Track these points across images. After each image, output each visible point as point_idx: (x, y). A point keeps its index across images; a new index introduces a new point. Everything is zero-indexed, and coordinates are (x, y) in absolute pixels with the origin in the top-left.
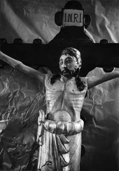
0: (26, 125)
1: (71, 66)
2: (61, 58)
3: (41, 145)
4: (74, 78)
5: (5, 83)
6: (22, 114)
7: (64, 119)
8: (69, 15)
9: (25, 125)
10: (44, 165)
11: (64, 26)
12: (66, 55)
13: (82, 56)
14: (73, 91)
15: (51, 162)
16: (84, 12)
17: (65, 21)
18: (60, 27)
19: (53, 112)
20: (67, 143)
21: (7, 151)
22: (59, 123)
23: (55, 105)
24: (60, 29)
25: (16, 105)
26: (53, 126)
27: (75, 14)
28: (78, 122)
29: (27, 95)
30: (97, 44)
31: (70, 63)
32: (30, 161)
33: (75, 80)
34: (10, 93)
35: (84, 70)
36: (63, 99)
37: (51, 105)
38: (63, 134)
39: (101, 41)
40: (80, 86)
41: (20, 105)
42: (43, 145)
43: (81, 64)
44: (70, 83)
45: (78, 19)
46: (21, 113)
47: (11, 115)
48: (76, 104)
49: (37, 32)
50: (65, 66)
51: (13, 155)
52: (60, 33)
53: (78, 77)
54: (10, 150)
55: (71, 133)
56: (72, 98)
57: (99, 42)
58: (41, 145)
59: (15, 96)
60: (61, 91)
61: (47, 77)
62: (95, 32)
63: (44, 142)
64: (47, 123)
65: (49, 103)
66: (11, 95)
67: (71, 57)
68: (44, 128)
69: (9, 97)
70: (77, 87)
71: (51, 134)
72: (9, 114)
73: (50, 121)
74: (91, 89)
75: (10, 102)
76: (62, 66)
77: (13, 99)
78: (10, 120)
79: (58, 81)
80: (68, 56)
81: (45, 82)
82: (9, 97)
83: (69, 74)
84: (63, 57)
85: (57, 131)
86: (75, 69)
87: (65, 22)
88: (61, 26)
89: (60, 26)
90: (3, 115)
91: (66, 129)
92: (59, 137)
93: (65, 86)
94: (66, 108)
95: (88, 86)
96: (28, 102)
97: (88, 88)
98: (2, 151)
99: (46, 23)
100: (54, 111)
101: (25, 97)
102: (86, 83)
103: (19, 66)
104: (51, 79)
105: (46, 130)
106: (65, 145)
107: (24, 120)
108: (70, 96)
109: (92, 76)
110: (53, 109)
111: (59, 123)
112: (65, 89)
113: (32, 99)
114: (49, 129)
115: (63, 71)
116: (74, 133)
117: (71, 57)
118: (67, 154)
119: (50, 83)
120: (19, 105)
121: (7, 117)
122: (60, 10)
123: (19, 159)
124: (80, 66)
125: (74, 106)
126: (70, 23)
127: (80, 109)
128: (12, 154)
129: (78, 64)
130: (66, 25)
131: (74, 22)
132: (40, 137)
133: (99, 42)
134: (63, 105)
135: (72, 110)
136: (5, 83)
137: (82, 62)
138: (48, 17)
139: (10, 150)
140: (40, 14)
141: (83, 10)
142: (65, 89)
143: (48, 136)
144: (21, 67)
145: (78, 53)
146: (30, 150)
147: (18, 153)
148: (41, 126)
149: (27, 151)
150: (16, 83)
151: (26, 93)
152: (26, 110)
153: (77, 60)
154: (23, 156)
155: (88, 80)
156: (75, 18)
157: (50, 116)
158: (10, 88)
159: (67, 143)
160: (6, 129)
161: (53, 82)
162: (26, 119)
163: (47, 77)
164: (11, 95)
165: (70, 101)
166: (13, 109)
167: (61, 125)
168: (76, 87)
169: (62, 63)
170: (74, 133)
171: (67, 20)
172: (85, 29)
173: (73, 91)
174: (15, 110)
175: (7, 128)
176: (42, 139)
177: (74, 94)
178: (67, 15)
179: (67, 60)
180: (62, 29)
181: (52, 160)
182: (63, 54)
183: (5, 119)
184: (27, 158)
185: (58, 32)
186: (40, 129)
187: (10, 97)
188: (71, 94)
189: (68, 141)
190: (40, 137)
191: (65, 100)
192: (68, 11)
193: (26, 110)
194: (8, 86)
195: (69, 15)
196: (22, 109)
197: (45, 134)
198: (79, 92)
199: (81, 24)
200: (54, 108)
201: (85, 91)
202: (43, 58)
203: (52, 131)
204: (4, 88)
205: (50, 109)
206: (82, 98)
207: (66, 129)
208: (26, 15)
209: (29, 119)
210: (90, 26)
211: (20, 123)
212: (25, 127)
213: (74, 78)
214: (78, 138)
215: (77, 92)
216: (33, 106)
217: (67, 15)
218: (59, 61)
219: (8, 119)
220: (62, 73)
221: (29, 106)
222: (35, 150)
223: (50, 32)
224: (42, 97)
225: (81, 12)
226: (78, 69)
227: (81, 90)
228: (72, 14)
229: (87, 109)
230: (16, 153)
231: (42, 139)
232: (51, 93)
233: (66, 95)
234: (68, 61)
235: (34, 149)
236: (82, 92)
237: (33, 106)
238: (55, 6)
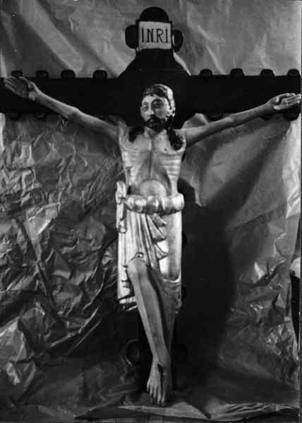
0: (91, 208)
1: (161, 113)
2: (143, 102)
3: (125, 233)
4: (165, 131)
5: (50, 144)
6: (83, 193)
7: (156, 192)
8: (149, 31)
9: (88, 208)
10: (132, 259)
11: (141, 49)
12: (152, 95)
13: (175, 96)
14: (166, 150)
15: (142, 253)
16: (172, 26)
17: (143, 41)
18: (133, 50)
19: (136, 184)
20: (163, 225)
21: (60, 253)
22: (150, 198)
23: (140, 174)
24: (135, 55)
25: (71, 177)
26: (141, 203)
27: (158, 30)
28: (177, 195)
29: (90, 161)
30: (194, 77)
31: (159, 107)
32: (99, 267)
33: (167, 134)
34: (61, 160)
35: (176, 122)
36: (151, 164)
37: (134, 173)
38: (157, 212)
39: (201, 72)
40: (175, 142)
41: (79, 178)
42: (127, 233)
43: (174, 109)
44: (160, 139)
45: (163, 37)
46: (81, 191)
47: (64, 194)
48: (172, 170)
49: (98, 59)
50: (153, 113)
51: (71, 257)
52: (135, 60)
53: (171, 129)
54: (65, 250)
55: (168, 212)
56: (165, 161)
57: (91, 76)
58: (125, 233)
59: (71, 164)
60: (147, 151)
61: (122, 131)
62: (190, 59)
63: (129, 227)
64: (130, 201)
65: (129, 171)
66: (63, 163)
67: (161, 99)
68: (126, 207)
69: (60, 165)
70: (171, 144)
71: (138, 215)
72: (60, 194)
73: (134, 196)
74: (189, 149)
75: (62, 173)
76: (147, 114)
77: (65, 169)
78: (63, 202)
79: (140, 137)
80: (155, 97)
81: (120, 139)
82: (60, 165)
83: (158, 124)
84: (148, 99)
85: (148, 210)
86: (167, 116)
87: (143, 44)
88: (138, 49)
89: (133, 48)
90: (50, 195)
91: (160, 206)
92: (151, 218)
93: (153, 143)
94: (158, 177)
95: (187, 142)
96: (93, 171)
97: (187, 146)
98: (50, 255)
99: (108, 43)
100: (139, 181)
101: (86, 164)
102: (184, 137)
103: (75, 115)
104: (130, 134)
105: (131, 210)
106: (160, 229)
107: (86, 201)
108: (161, 158)
109: (188, 131)
110: (137, 179)
111: (150, 198)
112: (154, 148)
113: (97, 167)
114: (136, 208)
115: (149, 120)
116: (173, 211)
117: (161, 99)
118: (164, 242)
119: (127, 140)
120: (76, 180)
121: (57, 199)
122: (133, 23)
123: (82, 262)
124: (174, 112)
125: (168, 172)
126: (150, 43)
127: (177, 178)
128: (70, 256)
129: (171, 108)
130: (144, 48)
131: (158, 41)
132: (121, 220)
133: (91, 76)
134: (152, 171)
135: (165, 178)
136: (50, 144)
137: (177, 105)
138: (110, 33)
139: (65, 250)
140: (97, 28)
141: (171, 22)
142: (154, 148)
143: (133, 216)
144: (80, 117)
145: (170, 92)
146: (100, 247)
147: (80, 254)
148: (122, 206)
149: (94, 249)
150: (68, 143)
151: (88, 157)
152: (88, 185)
153: (170, 104)
154: (87, 258)
155: (186, 133)
156: (158, 36)
157: (133, 189)
158: (59, 151)
159: (163, 225)
160: (57, 218)
161: (132, 138)
162: (90, 199)
163: (122, 131)
164: (63, 163)
165: (161, 165)
166: (67, 186)
167: (154, 200)
168: (169, 144)
169: (147, 108)
170: (173, 211)
171: (146, 39)
172: (175, 54)
173: (166, 150)
174: (70, 186)
175: (59, 215)
176: (125, 224)
177: (168, 155)
178: (145, 31)
179: (155, 103)
180: (138, 53)
181: (144, 251)
182: (148, 94)
183: (54, 202)
184: (94, 261)
185: (133, 59)
186: (120, 209)
187: (62, 166)
188: (163, 154)
189: (165, 223)
190: (121, 220)
191: (155, 165)
192: (146, 25)
193: (88, 185)
194: (55, 147)
195: (149, 31)
196: (82, 184)
197: (128, 215)
198: (175, 152)
199: (168, 46)
200: (140, 178)
201: (182, 150)
202: (112, 99)
203: (141, 210)
204: (48, 152)
205: (133, 179)
206: (178, 161)
207: (160, 206)
208: (75, 29)
209: (95, 200)
210: (182, 49)
211: (80, 208)
212: (88, 212)
213: (165, 131)
214: (178, 218)
215: (171, 152)
216: (99, 179)
217: (145, 31)
218: (140, 104)
219: (60, 201)
220: (147, 123)
221: (94, 179)
222: (107, 247)
223: (119, 61)
224: (114, 164)
225: (168, 26)
226: (171, 116)
227: (176, 148)
228: (152, 30)
229: (185, 178)
230: (75, 255)
231: (125, 224)
232: (131, 155)
233: (155, 156)
234: (157, 105)
235: (106, 244)
236: (179, 151)
237: (99, 179)
238: (121, 13)
